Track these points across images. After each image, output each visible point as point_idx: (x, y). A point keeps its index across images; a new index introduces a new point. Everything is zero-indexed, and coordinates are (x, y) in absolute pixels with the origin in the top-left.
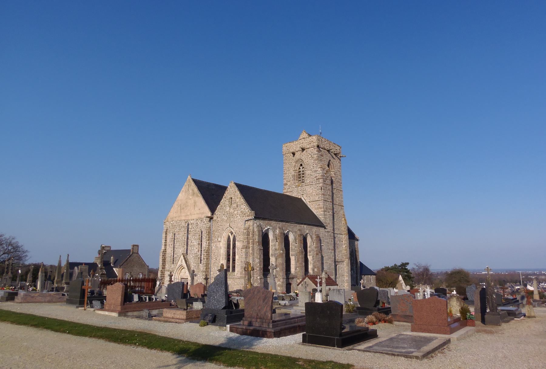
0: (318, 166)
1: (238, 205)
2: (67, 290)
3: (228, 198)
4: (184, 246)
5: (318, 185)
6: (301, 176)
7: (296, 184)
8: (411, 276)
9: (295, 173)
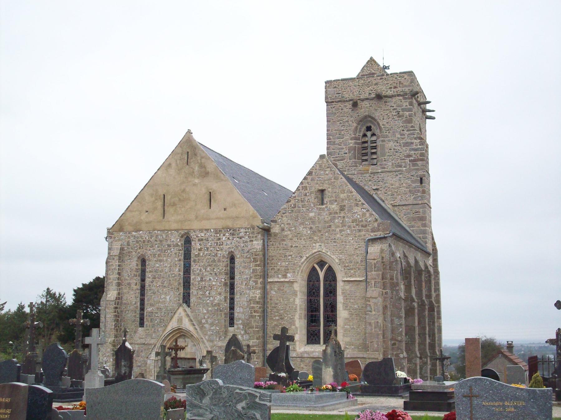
0: (414, 135)
1: (345, 206)
3: (313, 189)
4: (178, 289)
5: (413, 173)
6: (369, 151)
7: (357, 166)
9: (356, 143)
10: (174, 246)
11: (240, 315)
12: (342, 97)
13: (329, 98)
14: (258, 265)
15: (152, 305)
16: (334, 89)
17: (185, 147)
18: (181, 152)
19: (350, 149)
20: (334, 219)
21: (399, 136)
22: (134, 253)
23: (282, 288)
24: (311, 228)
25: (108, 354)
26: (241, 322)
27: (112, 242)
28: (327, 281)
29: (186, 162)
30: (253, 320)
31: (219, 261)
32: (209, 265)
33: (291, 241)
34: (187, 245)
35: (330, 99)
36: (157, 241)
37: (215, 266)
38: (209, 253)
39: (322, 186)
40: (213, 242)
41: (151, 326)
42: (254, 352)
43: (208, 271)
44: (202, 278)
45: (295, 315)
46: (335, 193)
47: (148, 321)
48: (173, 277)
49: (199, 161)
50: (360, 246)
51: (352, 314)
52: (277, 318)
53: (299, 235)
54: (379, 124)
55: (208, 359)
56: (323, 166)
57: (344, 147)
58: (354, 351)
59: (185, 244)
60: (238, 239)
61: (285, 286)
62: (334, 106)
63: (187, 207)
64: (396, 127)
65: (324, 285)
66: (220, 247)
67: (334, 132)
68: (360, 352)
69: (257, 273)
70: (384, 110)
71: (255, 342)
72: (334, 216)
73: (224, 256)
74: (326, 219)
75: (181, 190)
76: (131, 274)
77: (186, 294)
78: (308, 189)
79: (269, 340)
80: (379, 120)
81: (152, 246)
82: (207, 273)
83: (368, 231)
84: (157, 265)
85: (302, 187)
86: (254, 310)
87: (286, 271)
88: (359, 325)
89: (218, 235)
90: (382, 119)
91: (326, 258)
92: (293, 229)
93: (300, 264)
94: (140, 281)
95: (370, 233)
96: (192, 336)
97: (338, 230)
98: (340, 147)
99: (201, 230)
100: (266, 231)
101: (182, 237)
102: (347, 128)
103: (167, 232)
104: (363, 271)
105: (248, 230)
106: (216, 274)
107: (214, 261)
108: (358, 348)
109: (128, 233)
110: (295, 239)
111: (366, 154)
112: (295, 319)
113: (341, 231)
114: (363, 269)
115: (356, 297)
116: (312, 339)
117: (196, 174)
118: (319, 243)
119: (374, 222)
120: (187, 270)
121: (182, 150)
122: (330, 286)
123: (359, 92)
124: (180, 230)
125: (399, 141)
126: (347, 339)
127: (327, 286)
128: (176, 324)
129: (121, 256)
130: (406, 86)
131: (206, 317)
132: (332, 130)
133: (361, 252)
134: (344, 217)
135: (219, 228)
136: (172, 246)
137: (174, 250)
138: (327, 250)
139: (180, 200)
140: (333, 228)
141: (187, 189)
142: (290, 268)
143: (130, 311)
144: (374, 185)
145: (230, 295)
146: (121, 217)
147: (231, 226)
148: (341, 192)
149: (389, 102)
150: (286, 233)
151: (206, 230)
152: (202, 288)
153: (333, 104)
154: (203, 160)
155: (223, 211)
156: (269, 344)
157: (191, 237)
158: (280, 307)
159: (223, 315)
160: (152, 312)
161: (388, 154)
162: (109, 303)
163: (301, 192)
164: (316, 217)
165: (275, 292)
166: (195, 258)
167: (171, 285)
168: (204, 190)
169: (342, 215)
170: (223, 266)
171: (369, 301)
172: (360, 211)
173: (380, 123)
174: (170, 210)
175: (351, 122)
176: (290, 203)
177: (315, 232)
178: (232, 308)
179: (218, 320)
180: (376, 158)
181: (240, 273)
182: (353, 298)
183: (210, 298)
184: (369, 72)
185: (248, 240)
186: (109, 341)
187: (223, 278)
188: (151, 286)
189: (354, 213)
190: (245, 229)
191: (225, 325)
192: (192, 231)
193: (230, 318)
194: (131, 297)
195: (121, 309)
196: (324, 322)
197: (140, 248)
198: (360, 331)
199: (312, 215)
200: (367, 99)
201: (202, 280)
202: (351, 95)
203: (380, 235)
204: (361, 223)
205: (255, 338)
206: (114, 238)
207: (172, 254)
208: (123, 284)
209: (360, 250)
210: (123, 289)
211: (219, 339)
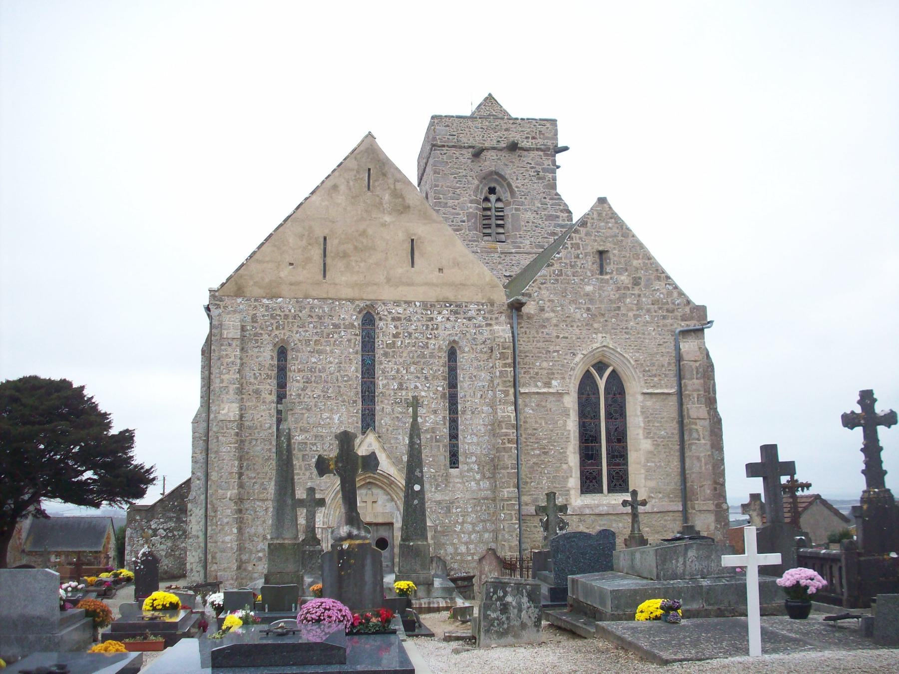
1: (640, 278)
2: (594, 588)
6: (493, 222)
9: (477, 208)
11: (473, 449)
12: (458, 141)
13: (439, 140)
15: (303, 430)
16: (445, 128)
17: (364, 160)
18: (356, 167)
19: (469, 215)
20: (624, 298)
21: (540, 205)
22: (266, 337)
23: (543, 404)
24: (588, 309)
25: (228, 519)
26: (474, 459)
28: (609, 394)
29: (367, 185)
30: (506, 455)
31: (432, 356)
32: (414, 363)
33: (556, 328)
34: (368, 327)
35: (440, 142)
36: (312, 317)
37: (424, 363)
38: (413, 341)
39: (604, 246)
40: (419, 324)
41: (303, 468)
43: (412, 373)
44: (401, 384)
45: (566, 448)
46: (624, 257)
48: (346, 381)
49: (392, 187)
50: (665, 340)
51: (658, 445)
52: (537, 452)
53: (570, 320)
54: (509, 185)
55: (755, 510)
56: (604, 215)
57: (461, 212)
58: (662, 501)
59: (363, 324)
60: (465, 320)
61: (549, 401)
62: (445, 152)
63: (371, 261)
64: (535, 191)
66: (432, 332)
67: (446, 188)
68: (672, 503)
69: (507, 377)
70: (518, 167)
72: (624, 294)
73: (440, 349)
74: (612, 297)
75: (357, 231)
76: (260, 374)
77: (367, 412)
78: (581, 248)
79: (525, 488)
81: (303, 326)
82: (410, 377)
83: (675, 318)
84: (314, 360)
85: (572, 244)
86: (508, 439)
87: (551, 375)
88: (669, 462)
89: (429, 313)
90: (515, 178)
91: (613, 357)
92: (558, 309)
93: (572, 365)
95: (680, 322)
96: (392, 483)
97: (631, 314)
99: (397, 303)
101: (360, 312)
102: (465, 186)
103: (331, 301)
104: (673, 379)
105: (483, 306)
106: (426, 378)
108: (669, 497)
109: (252, 300)
110: (563, 325)
111: (488, 226)
112: (568, 453)
113: (636, 317)
114: (672, 376)
115: (662, 418)
116: (615, 485)
117: (385, 206)
118: (601, 333)
120: (368, 370)
121: (358, 165)
122: (615, 401)
123: (483, 137)
124: (358, 300)
125: (539, 213)
126: (652, 484)
127: (610, 402)
130: (547, 138)
132: (442, 186)
133: (667, 350)
134: (639, 296)
135: (431, 300)
138: (616, 345)
139: (356, 248)
140: (623, 310)
141: (370, 231)
143: (259, 442)
144: (506, 271)
145: (450, 414)
146: (238, 270)
147: (452, 298)
148: (634, 257)
149: (524, 157)
150: (547, 315)
151: (406, 302)
152: (401, 402)
153: (443, 148)
154: (399, 186)
155: (437, 273)
156: (524, 495)
158: (541, 434)
159: (441, 448)
160: (306, 444)
162: (226, 426)
163: (570, 252)
164: (595, 293)
166: (387, 350)
167: (342, 395)
168: (401, 235)
170: (439, 365)
171: (696, 424)
172: (663, 289)
173: (513, 184)
174: (336, 266)
175: (471, 178)
176: (552, 268)
178: (454, 436)
180: (503, 233)
181: (470, 378)
182: (659, 420)
184: (489, 112)
185: (484, 323)
186: (229, 496)
187: (441, 386)
189: (655, 290)
190: (478, 305)
192: (380, 303)
194: (262, 416)
195: (241, 436)
197: (277, 328)
198: (671, 471)
199: (589, 288)
200: (494, 148)
202: (471, 139)
203: (695, 326)
204: (666, 307)
205: (512, 485)
206: (224, 307)
207: (341, 341)
208: (244, 391)
209: (665, 348)
210: (245, 400)
211: (436, 488)
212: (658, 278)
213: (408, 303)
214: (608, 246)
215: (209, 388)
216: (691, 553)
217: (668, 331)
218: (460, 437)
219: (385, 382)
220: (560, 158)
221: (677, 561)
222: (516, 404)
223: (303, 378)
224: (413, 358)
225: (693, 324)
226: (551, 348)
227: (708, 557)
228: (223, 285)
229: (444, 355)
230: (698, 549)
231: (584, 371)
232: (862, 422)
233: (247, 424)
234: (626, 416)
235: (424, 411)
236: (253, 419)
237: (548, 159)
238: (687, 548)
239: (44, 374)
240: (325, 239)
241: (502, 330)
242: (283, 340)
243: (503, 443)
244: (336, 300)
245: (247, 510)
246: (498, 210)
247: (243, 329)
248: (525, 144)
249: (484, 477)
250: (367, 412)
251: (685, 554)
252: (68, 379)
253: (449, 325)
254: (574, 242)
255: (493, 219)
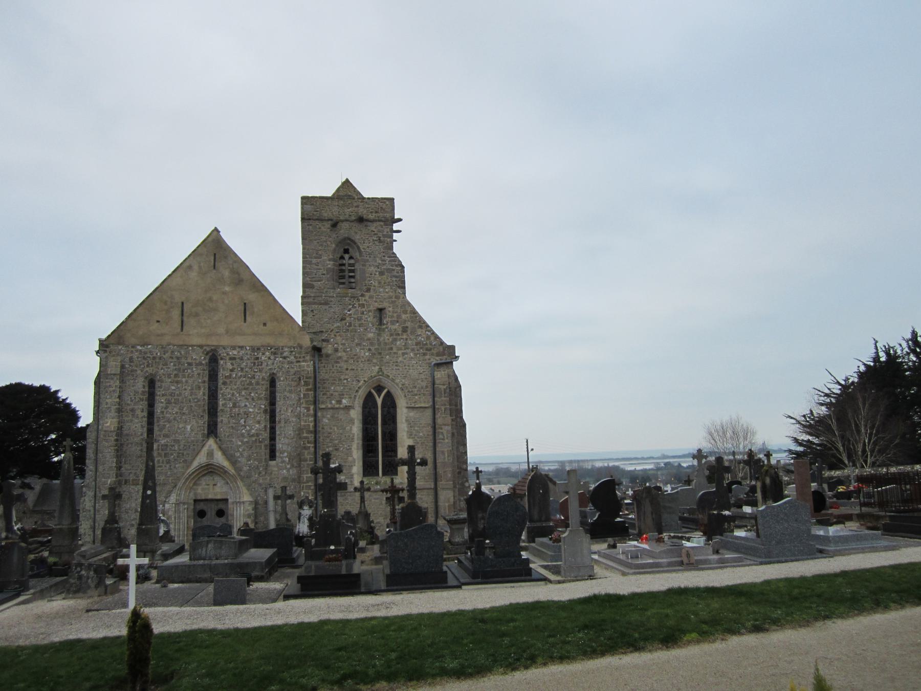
1: (407, 327)
3: (371, 308)
8: (917, 470)
10: (197, 365)
14: (310, 390)
15: (166, 436)
21: (380, 262)
22: (139, 372)
24: (370, 350)
26: (286, 454)
27: (106, 357)
30: (306, 452)
31: (258, 383)
32: (245, 389)
37: (252, 389)
40: (249, 362)
41: (165, 462)
42: (356, 489)
43: (243, 396)
47: (161, 456)
53: (356, 357)
54: (358, 248)
57: (322, 268)
59: (210, 362)
65: (382, 411)
71: (309, 477)
77: (212, 423)
80: (359, 244)
81: (166, 364)
82: (242, 398)
83: (432, 354)
84: (173, 388)
87: (342, 395)
94: (147, 407)
96: (226, 472)
98: (317, 267)
99: (234, 348)
100: (317, 350)
101: (207, 354)
106: (253, 399)
107: (251, 384)
108: (425, 479)
109: (130, 346)
111: (343, 277)
113: (403, 354)
116: (388, 471)
119: (439, 346)
120: (213, 395)
123: (339, 212)
128: (205, 459)
129: (123, 375)
131: (240, 450)
134: (407, 339)
136: (194, 364)
137: (196, 370)
140: (395, 350)
141: (215, 298)
142: (345, 393)
145: (270, 423)
150: (340, 354)
151: (239, 347)
155: (261, 326)
157: (220, 355)
160: (167, 445)
161: (369, 279)
163: (357, 310)
165: (329, 420)
169: (405, 337)
170: (262, 391)
171: (442, 429)
176: (345, 321)
177: (375, 354)
178: (273, 438)
179: (257, 453)
181: (284, 398)
183: (246, 427)
187: (263, 404)
188: (165, 413)
189: (417, 335)
191: (265, 459)
192: (221, 348)
193: (270, 450)
196: (382, 452)
197: (148, 366)
199: (371, 335)
200: (347, 220)
201: (235, 406)
212: (420, 327)
213: (241, 347)
214: (385, 305)
215: (98, 408)
216: (210, 546)
217: (427, 363)
218: (277, 439)
219: (224, 402)
220: (396, 227)
221: (202, 550)
222: (315, 415)
223: (165, 400)
224: (244, 385)
225: (444, 359)
226: (342, 377)
227: (221, 548)
228: (109, 336)
229: (266, 384)
230: (215, 544)
231: (366, 393)
232: (321, 471)
233: (125, 432)
234: (396, 422)
235: (251, 422)
236: (130, 429)
237: (387, 228)
238: (208, 542)
239: (27, 382)
240: (183, 303)
241: (307, 366)
242: (151, 374)
243: (304, 444)
244: (190, 346)
245: (125, 491)
246: (350, 265)
247: (123, 367)
248: (371, 217)
249: (292, 466)
250: (212, 423)
251: (207, 546)
252: (47, 385)
253: (270, 362)
254: (361, 302)
255: (347, 272)
